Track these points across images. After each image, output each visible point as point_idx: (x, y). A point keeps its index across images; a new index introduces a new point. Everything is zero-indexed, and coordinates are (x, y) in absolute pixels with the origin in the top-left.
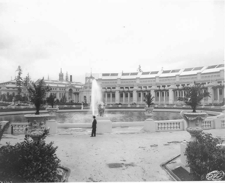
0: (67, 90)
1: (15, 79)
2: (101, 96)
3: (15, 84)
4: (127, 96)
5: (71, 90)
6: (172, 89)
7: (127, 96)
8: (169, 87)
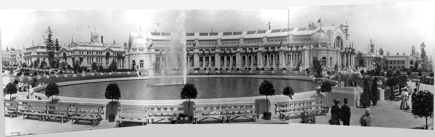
0: (104, 54)
1: (46, 42)
2: (393, 53)
3: (44, 48)
4: (207, 58)
5: (108, 54)
7: (228, 59)
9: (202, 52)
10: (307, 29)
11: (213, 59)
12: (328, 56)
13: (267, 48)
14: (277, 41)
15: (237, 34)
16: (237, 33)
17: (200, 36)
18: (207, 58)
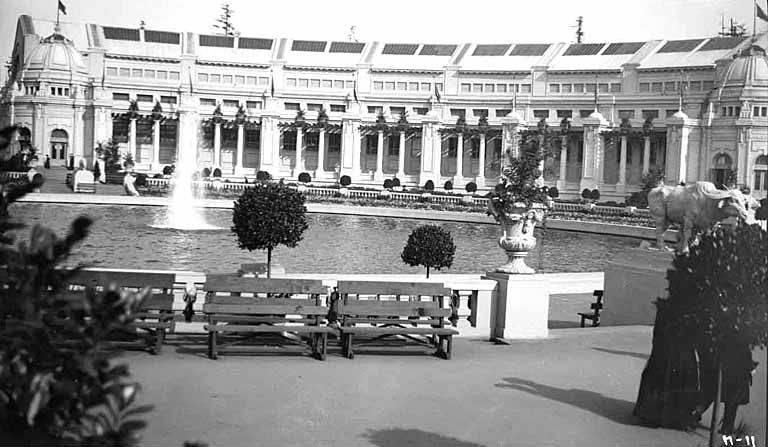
4: (311, 141)
6: (277, 122)
8: (587, 121)
9: (293, 113)
10: (700, 46)
11: (335, 142)
12: (75, 127)
13: (542, 114)
14: (585, 89)
15: (436, 53)
16: (436, 49)
17: (293, 49)
18: (311, 141)
